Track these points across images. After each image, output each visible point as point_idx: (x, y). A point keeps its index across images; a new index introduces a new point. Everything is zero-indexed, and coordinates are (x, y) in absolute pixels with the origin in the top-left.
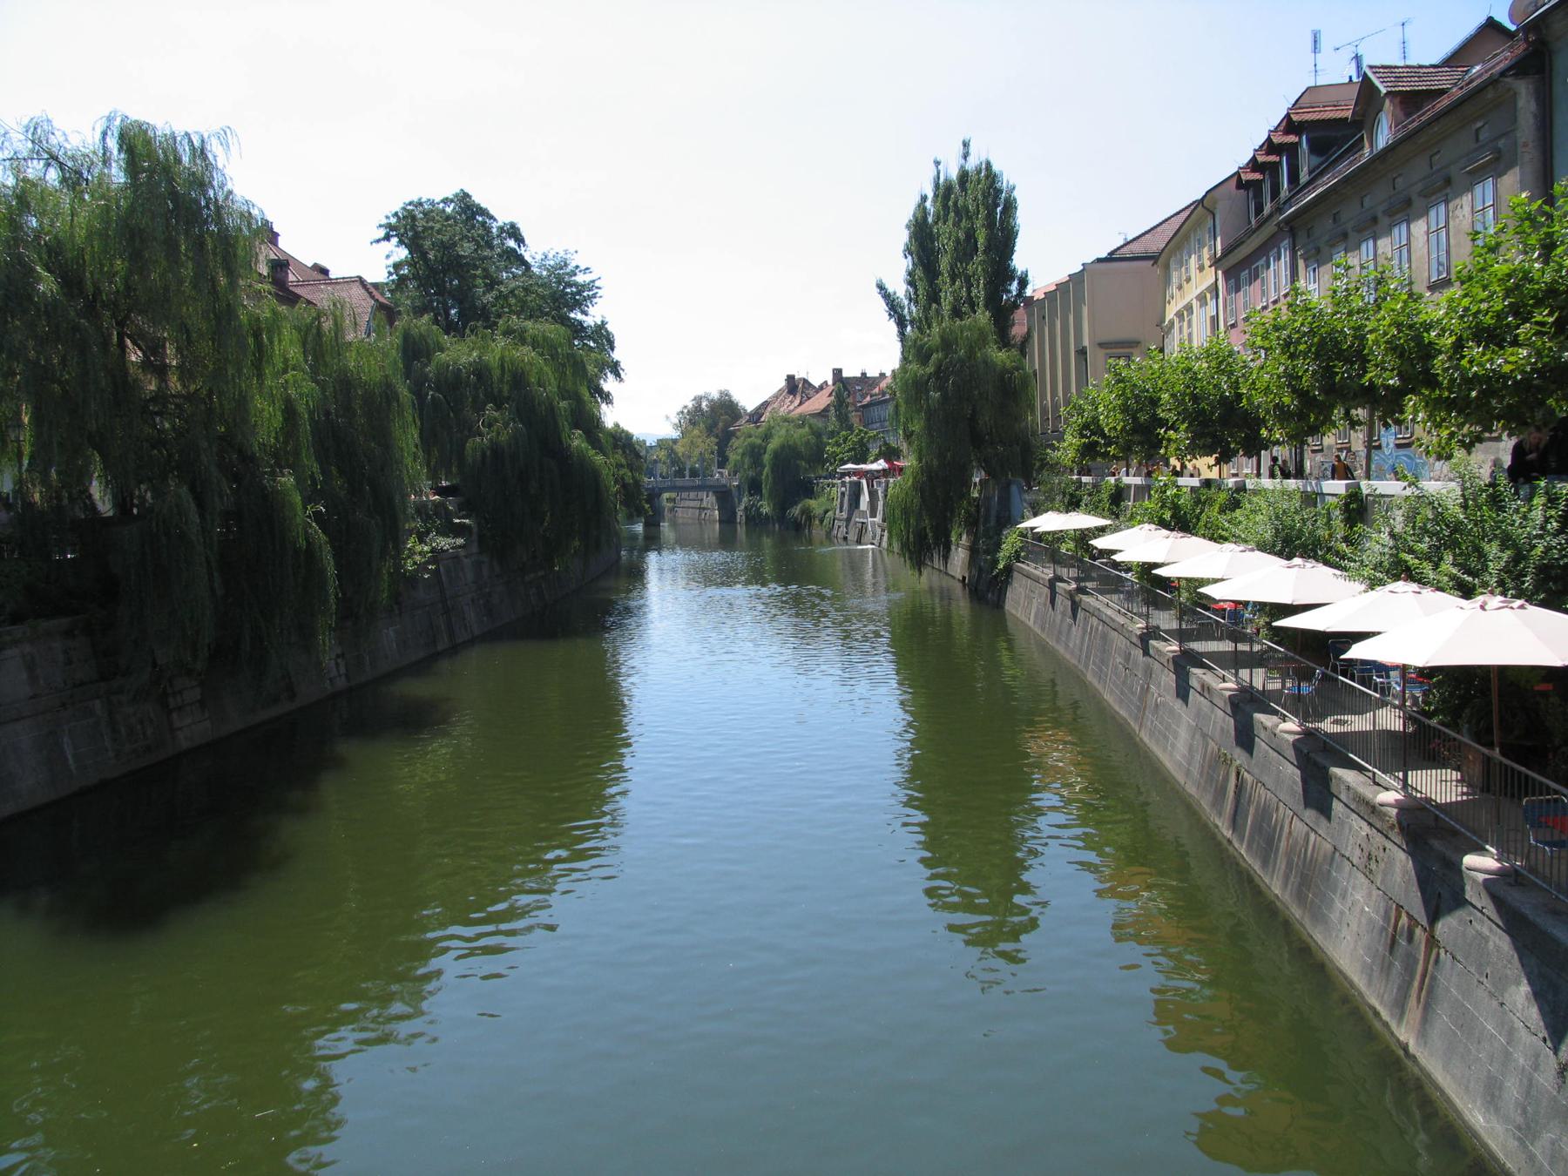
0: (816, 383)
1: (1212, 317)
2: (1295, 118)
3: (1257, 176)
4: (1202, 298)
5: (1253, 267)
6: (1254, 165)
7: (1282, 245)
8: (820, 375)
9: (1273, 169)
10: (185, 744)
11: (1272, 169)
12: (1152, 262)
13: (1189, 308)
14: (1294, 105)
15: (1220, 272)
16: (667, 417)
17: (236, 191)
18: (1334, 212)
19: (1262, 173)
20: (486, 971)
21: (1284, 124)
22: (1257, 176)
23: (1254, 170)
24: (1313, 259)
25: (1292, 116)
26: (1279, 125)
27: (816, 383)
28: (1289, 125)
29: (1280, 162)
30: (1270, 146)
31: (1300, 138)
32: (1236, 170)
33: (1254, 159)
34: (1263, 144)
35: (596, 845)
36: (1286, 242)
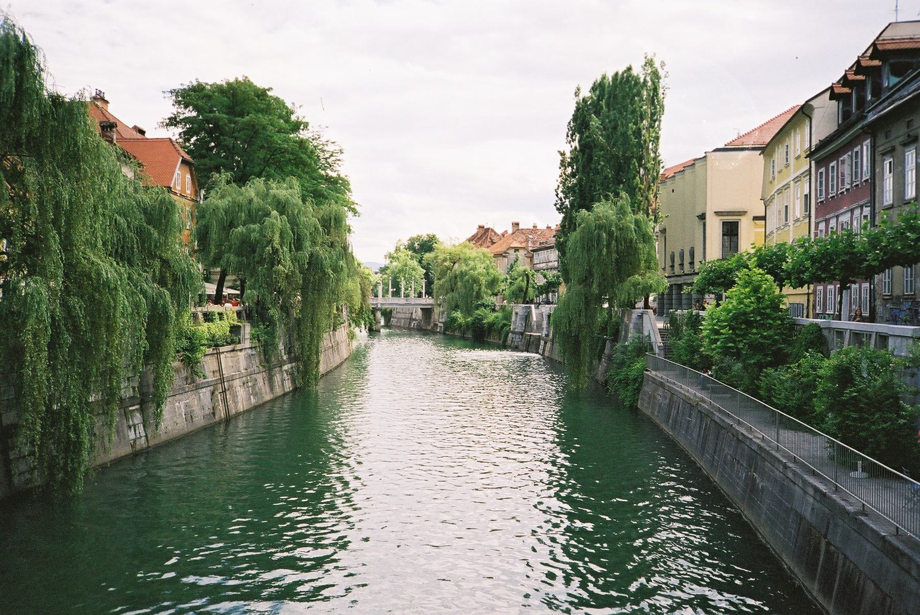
0: (499, 231)
1: (806, 196)
2: (880, 47)
3: (846, 90)
4: (797, 180)
5: (841, 159)
6: (845, 81)
7: (865, 143)
8: (501, 226)
9: (860, 85)
10: (164, 437)
11: (859, 86)
12: (759, 152)
13: (787, 186)
14: (863, 54)
15: (813, 162)
16: (399, 241)
17: (62, 92)
18: (907, 120)
19: (851, 88)
20: (398, 445)
21: (870, 51)
22: (846, 90)
23: (844, 86)
24: (889, 155)
25: (848, 75)
26: (866, 52)
27: (499, 231)
28: (876, 50)
29: (851, 94)
30: (858, 67)
31: (852, 91)
32: (831, 85)
33: (845, 77)
34: (852, 67)
35: (679, 278)
36: (868, 141)
